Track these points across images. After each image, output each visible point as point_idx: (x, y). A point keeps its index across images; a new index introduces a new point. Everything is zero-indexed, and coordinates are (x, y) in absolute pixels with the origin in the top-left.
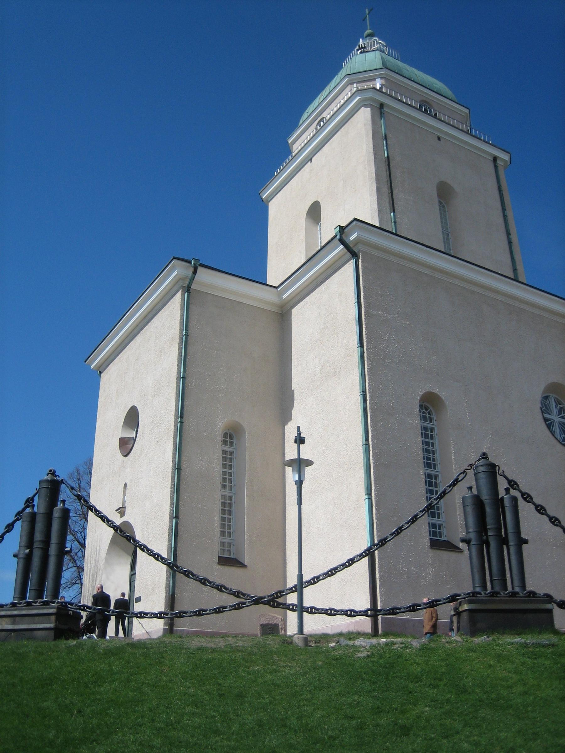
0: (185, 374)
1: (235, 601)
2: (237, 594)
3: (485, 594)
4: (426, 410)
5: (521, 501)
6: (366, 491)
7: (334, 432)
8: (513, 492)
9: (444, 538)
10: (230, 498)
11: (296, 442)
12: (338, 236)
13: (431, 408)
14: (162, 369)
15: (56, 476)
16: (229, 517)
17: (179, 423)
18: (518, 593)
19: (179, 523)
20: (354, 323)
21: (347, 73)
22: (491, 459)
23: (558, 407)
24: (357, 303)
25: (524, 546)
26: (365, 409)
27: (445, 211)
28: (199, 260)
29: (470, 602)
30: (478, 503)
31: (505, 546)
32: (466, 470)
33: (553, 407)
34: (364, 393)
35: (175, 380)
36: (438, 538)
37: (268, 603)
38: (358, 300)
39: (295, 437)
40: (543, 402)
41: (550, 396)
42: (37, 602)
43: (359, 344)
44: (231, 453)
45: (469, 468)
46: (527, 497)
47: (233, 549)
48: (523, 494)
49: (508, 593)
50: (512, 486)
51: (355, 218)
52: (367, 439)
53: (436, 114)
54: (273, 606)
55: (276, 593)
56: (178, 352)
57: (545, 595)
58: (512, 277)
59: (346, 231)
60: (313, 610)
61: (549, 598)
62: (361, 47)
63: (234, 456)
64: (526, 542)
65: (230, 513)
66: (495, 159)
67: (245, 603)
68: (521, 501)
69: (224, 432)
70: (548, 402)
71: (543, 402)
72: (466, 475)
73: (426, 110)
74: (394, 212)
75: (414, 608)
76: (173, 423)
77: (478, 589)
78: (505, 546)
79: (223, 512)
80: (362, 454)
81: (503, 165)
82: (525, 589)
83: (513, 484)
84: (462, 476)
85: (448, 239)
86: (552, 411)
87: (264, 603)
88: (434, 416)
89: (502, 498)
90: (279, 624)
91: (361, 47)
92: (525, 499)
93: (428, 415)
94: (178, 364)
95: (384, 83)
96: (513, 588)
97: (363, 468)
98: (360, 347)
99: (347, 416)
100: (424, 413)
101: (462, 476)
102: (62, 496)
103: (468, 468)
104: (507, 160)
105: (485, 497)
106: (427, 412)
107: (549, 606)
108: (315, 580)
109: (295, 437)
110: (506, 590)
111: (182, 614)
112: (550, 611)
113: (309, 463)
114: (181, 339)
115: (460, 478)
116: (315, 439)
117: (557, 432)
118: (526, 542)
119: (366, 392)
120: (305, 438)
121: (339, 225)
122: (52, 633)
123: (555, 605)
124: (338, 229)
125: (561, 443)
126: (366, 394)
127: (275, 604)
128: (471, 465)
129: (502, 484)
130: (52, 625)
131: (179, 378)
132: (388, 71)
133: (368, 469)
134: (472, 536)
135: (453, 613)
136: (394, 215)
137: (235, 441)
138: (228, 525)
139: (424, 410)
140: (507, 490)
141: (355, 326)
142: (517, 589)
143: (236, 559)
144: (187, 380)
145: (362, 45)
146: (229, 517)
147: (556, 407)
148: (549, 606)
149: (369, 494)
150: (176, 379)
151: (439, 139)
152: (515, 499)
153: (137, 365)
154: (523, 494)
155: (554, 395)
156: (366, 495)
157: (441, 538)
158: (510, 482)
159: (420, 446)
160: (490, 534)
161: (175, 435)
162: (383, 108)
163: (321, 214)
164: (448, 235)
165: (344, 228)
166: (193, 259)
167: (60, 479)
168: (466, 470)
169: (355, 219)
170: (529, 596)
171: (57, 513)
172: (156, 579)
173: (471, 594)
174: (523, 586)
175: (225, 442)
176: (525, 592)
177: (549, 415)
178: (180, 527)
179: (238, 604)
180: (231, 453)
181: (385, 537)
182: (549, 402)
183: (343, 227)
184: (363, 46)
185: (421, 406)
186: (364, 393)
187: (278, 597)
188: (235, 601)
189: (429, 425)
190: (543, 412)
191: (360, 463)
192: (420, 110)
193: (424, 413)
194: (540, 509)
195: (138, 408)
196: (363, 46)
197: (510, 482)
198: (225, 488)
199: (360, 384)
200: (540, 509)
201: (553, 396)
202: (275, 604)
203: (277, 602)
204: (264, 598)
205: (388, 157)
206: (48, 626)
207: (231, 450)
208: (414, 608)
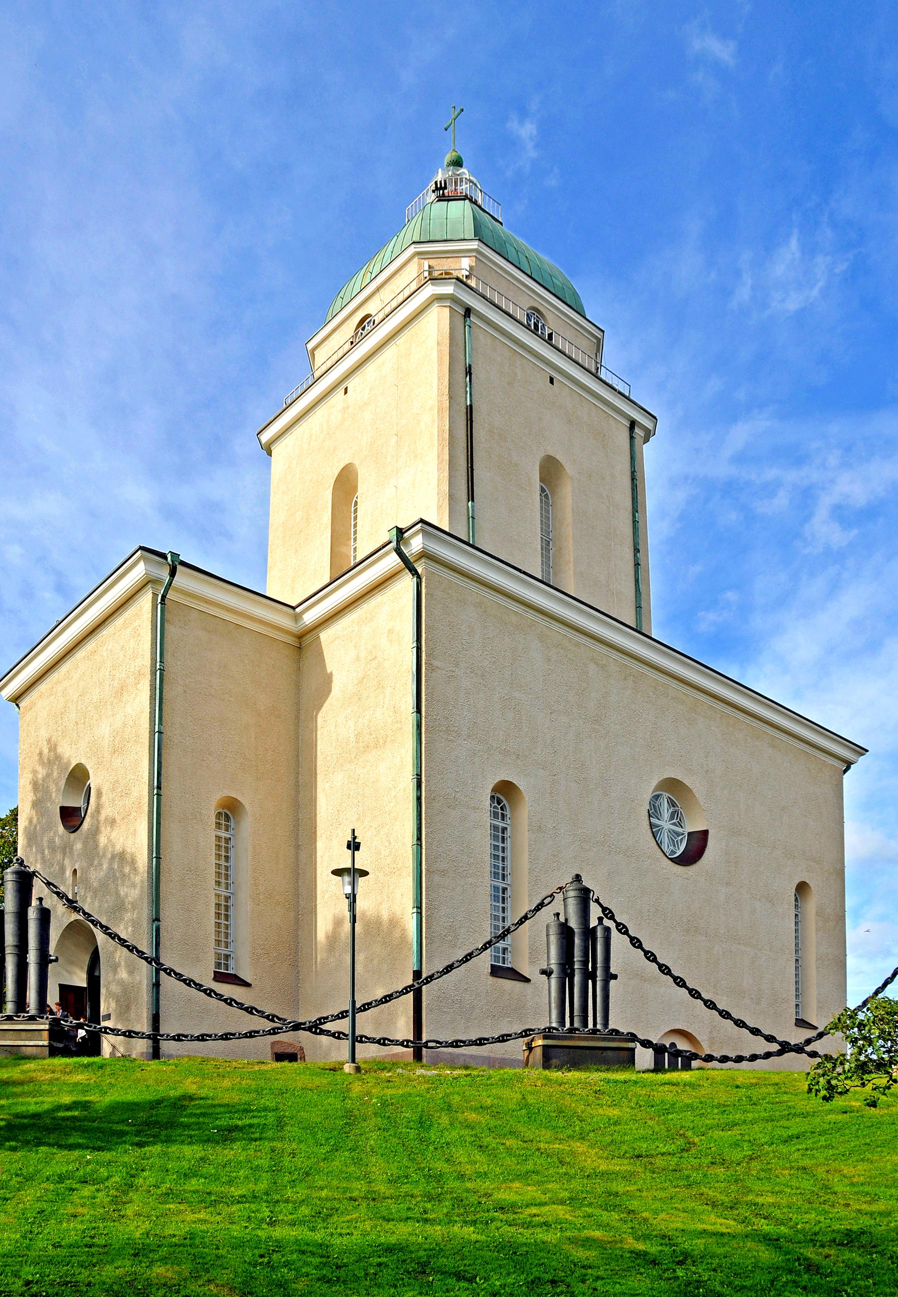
0: (162, 727)
1: (268, 1025)
2: (271, 1018)
3: (563, 1030)
4: (499, 803)
5: (614, 933)
6: (414, 903)
7: (372, 825)
8: (607, 922)
9: (508, 964)
10: (227, 899)
11: (349, 847)
12: (394, 544)
13: (505, 802)
14: (124, 716)
15: (25, 867)
16: (226, 923)
17: (156, 796)
18: (599, 1031)
19: (161, 927)
20: (411, 677)
21: (414, 239)
22: (587, 883)
23: (670, 811)
24: (415, 648)
25: (612, 983)
26: (419, 799)
27: (547, 504)
28: (179, 555)
29: (545, 1038)
30: (565, 932)
31: (590, 982)
32: (554, 894)
33: (664, 810)
34: (419, 777)
35: (147, 735)
36: (501, 964)
37: (309, 1029)
38: (417, 644)
39: (348, 841)
40: (652, 802)
41: (662, 795)
42: (20, 1016)
43: (415, 709)
44: (228, 840)
45: (559, 891)
46: (623, 929)
47: (231, 962)
48: (618, 924)
49: (589, 1030)
50: (606, 916)
51: (421, 519)
52: (419, 839)
53: (550, 335)
54: (315, 1033)
55: (319, 1019)
56: (149, 693)
57: (628, 1033)
58: (631, 621)
59: (406, 535)
60: (363, 1038)
61: (633, 1037)
62: (439, 186)
63: (232, 842)
64: (615, 977)
65: (227, 917)
66: (633, 424)
67: (281, 1029)
68: (614, 933)
69: (217, 812)
70: (658, 803)
71: (652, 802)
72: (553, 899)
73: (536, 325)
74: (473, 500)
75: (503, 1039)
76: (147, 795)
77: (554, 1025)
78: (590, 982)
79: (218, 915)
80: (411, 856)
81: (643, 435)
82: (607, 1028)
83: (608, 913)
84: (549, 899)
85: (548, 551)
86: (663, 816)
87: (304, 1029)
88: (508, 813)
89: (595, 928)
90: (297, 1054)
91: (439, 186)
92: (620, 931)
93: (500, 811)
94: (150, 712)
95: (474, 264)
96: (595, 1024)
97: (411, 874)
98: (417, 712)
99: (392, 804)
100: (495, 807)
101: (549, 899)
102: (35, 894)
103: (557, 891)
104: (651, 428)
105: (573, 923)
106: (499, 807)
107: (631, 1045)
108: (366, 1007)
109: (348, 841)
110: (587, 1027)
111: (253, 1034)
112: (633, 1050)
113: (364, 873)
114: (153, 673)
115: (546, 902)
116: (345, 831)
117: (664, 843)
118: (615, 977)
119: (421, 775)
120: (360, 843)
121: (396, 526)
122: (47, 1050)
123: (638, 1044)
124: (394, 531)
125: (666, 856)
126: (421, 778)
127: (318, 1031)
128: (561, 888)
129: (595, 912)
130: (46, 1043)
131: (152, 732)
132: (481, 245)
133: (418, 877)
134: (554, 967)
135: (524, 1048)
136: (473, 507)
137: (232, 824)
138: (224, 932)
139: (496, 804)
140: (600, 919)
141: (410, 681)
142: (599, 1027)
143: (235, 975)
144: (164, 736)
145: (441, 182)
146: (226, 923)
147: (668, 810)
148: (631, 1045)
149: (419, 907)
150: (148, 733)
151: (552, 381)
152: (607, 930)
153: (82, 704)
154: (618, 924)
155: (667, 795)
156: (413, 908)
157: (504, 964)
158: (604, 909)
159: (488, 850)
160: (576, 967)
161: (151, 812)
162: (469, 317)
163: (359, 487)
164: (548, 544)
165: (403, 531)
166: (170, 552)
167: (32, 870)
168: (554, 894)
169: (422, 521)
170: (611, 1034)
171: (32, 914)
172: (132, 995)
173: (547, 1030)
174: (606, 1023)
175: (218, 825)
176: (586, 1030)
177: (657, 820)
178: (163, 933)
179: (273, 1029)
180: (228, 840)
181: (451, 963)
182: (668, 847)
183: (401, 529)
184: (443, 185)
185: (492, 797)
186: (419, 777)
187: (322, 1024)
188: (268, 1025)
189: (501, 824)
190: (650, 816)
191: (408, 867)
192: (528, 327)
193: (495, 807)
194: (636, 943)
195: (88, 767)
196: (443, 185)
197: (604, 909)
198: (219, 885)
199: (413, 764)
200: (636, 943)
201: (666, 795)
202: (318, 1031)
203: (320, 1028)
204: (304, 1024)
205: (471, 406)
206: (41, 1043)
207: (228, 836)
208: (503, 1039)
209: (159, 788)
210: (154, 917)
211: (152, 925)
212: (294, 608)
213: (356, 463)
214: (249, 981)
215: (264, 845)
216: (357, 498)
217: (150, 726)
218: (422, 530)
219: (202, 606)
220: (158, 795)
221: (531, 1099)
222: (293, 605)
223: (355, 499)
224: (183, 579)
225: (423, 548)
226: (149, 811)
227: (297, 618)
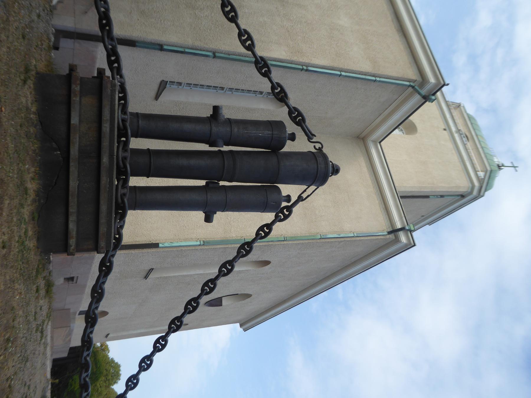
35: (341, 66)
120: (221, 305)
209: (307, 70)
210: (217, 54)
211: (211, 52)
212: (380, 142)
213: (417, 135)
214: (160, 99)
215: (254, 115)
216: (403, 133)
217: (345, 69)
218: (410, 244)
219: (398, 101)
220: (302, 69)
221: (30, 262)
222: (382, 143)
223: (404, 132)
224: (417, 98)
225: (401, 242)
226: (293, 61)
227: (375, 142)
